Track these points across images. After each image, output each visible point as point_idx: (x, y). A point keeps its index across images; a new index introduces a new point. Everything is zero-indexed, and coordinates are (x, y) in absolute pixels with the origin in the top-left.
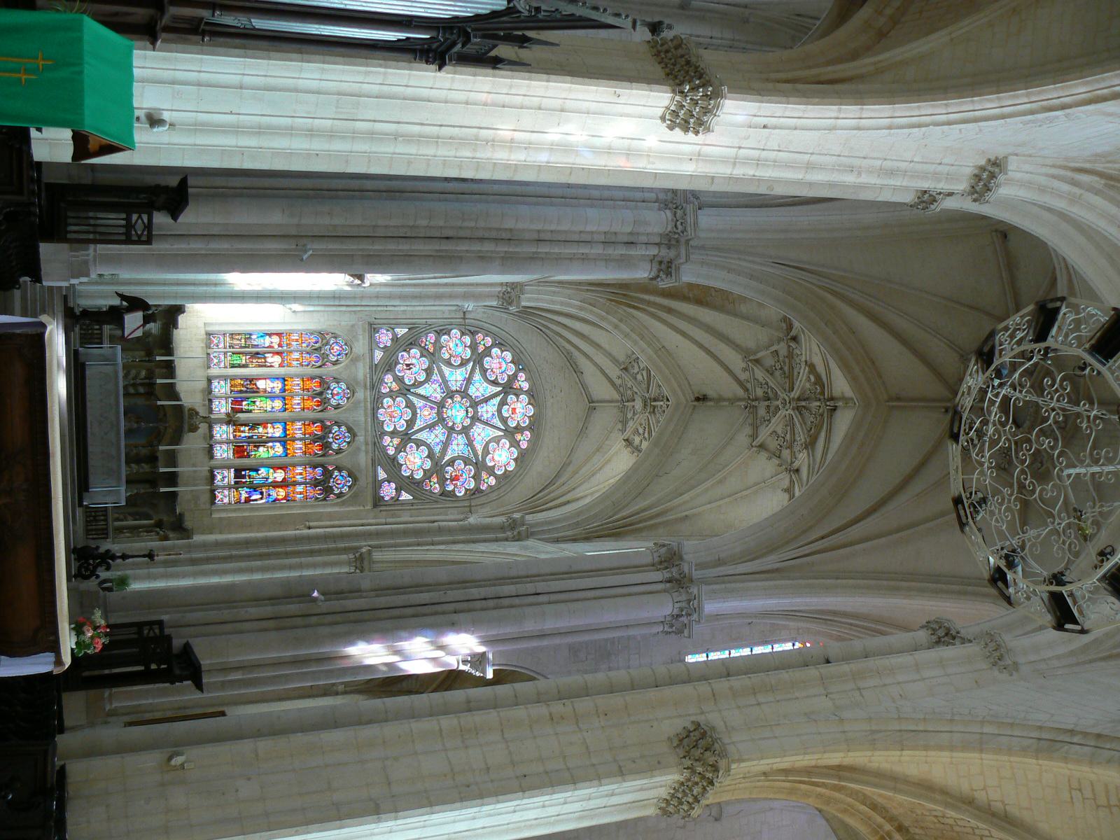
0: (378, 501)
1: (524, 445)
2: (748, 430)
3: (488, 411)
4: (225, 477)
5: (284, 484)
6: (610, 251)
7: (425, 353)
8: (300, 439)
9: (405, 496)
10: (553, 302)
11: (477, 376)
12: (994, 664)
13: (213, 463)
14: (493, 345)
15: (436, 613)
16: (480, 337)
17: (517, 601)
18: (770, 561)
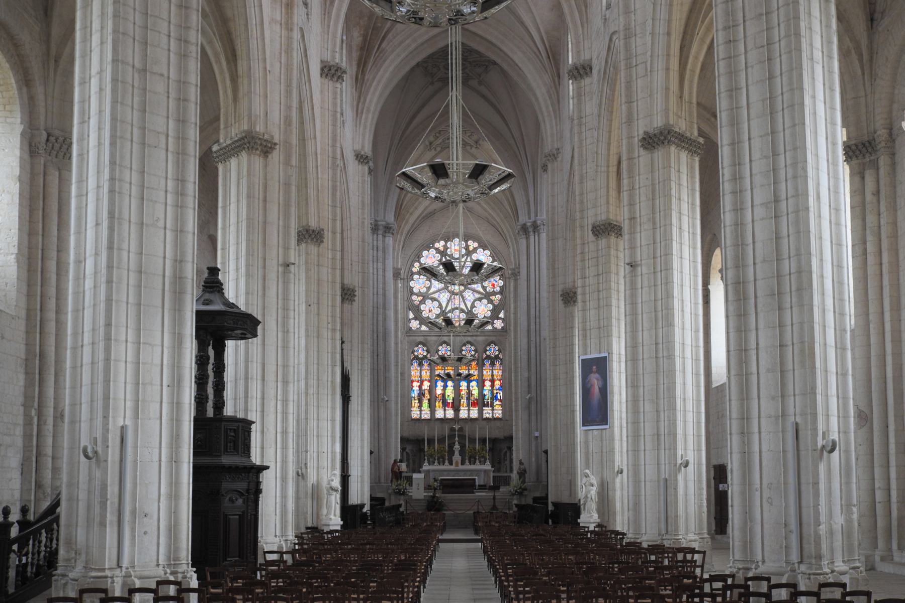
0: (504, 330)
1: (476, 245)
4: (487, 412)
5: (492, 382)
7: (423, 302)
9: (502, 315)
12: (556, 159)
15: (540, 346)
17: (537, 308)
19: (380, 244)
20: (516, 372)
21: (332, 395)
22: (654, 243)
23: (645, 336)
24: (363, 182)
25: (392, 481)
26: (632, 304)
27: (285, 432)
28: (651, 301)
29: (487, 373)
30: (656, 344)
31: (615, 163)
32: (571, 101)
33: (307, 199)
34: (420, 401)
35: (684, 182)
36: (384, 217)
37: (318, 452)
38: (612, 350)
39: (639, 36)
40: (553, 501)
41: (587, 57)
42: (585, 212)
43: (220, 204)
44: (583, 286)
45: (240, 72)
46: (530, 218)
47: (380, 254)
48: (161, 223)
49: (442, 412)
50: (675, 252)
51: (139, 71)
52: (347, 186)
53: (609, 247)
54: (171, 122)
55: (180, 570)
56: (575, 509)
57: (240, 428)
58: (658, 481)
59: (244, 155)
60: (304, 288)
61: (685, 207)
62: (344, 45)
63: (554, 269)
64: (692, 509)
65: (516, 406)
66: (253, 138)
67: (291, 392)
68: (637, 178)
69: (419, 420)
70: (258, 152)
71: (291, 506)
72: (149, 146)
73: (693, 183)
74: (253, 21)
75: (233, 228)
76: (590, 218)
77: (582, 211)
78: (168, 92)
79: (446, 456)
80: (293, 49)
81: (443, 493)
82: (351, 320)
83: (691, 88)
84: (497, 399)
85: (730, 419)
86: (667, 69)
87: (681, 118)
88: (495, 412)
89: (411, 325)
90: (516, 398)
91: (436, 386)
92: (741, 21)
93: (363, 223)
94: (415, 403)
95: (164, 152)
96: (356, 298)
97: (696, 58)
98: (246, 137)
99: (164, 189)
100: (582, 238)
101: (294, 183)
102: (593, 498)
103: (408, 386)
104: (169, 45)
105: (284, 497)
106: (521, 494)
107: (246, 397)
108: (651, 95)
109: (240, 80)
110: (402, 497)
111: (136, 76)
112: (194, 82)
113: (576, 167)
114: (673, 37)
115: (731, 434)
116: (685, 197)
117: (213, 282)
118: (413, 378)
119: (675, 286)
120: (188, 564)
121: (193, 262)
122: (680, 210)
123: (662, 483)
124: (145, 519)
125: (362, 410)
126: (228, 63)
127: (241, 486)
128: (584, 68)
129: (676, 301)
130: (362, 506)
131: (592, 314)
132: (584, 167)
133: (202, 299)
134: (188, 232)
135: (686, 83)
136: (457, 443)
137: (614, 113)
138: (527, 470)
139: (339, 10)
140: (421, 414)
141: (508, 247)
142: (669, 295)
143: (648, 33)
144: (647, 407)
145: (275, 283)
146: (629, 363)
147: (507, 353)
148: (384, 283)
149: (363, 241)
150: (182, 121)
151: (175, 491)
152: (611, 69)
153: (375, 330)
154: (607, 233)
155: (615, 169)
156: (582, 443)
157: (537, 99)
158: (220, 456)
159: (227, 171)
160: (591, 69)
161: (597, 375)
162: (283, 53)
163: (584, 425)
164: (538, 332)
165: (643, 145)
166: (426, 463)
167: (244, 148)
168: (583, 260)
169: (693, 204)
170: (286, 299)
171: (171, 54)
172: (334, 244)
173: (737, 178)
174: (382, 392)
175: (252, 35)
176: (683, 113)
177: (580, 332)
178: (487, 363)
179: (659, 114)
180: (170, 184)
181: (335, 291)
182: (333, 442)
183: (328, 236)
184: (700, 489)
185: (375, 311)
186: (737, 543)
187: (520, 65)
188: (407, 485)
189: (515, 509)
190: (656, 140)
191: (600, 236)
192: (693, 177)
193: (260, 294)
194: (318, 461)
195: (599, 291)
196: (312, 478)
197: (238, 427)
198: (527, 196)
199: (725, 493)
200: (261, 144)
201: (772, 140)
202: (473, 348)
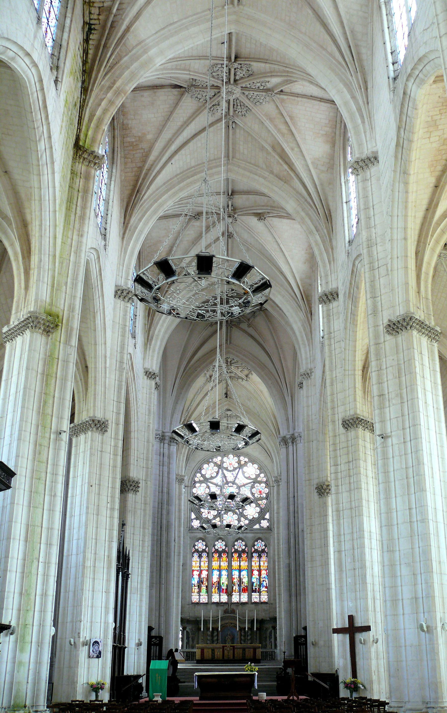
2: (240, 380)
3: (230, 477)
4: (255, 597)
5: (260, 571)
6: (166, 464)
8: (240, 563)
9: (267, 516)
10: (184, 453)
11: (214, 481)
12: (309, 377)
13: (250, 603)
14: (200, 473)
16: (197, 479)
18: (288, 399)
19: (166, 451)
21: (108, 568)
24: (150, 393)
26: (385, 473)
28: (402, 468)
34: (199, 587)
39: (380, 244)
41: (334, 286)
42: (336, 409)
45: (32, 266)
46: (289, 432)
47: (166, 459)
49: (218, 597)
52: (136, 395)
53: (357, 437)
60: (87, 471)
66: (37, 318)
68: (384, 359)
69: (198, 604)
76: (340, 414)
77: (333, 408)
80: (81, 251)
83: (426, 287)
88: (262, 597)
89: (193, 524)
90: (279, 584)
94: (196, 589)
96: (140, 489)
97: (429, 264)
98: (30, 317)
100: (334, 430)
101: (72, 361)
103: (190, 575)
109: (32, 272)
113: (327, 373)
114: (409, 241)
125: (142, 588)
126: (23, 258)
128: (332, 294)
131: (344, 497)
132: (334, 372)
140: (199, 598)
141: (273, 462)
142: (419, 462)
147: (271, 548)
149: (148, 442)
154: (355, 426)
156: (338, 615)
157: (294, 333)
159: (13, 349)
160: (338, 295)
172: (117, 434)
175: (44, 234)
176: (421, 305)
177: (334, 513)
181: (116, 475)
182: (107, 613)
183: (111, 427)
185: (160, 506)
187: (280, 306)
190: (400, 326)
191: (349, 429)
195: (350, 476)
198: (286, 414)
202: (244, 543)
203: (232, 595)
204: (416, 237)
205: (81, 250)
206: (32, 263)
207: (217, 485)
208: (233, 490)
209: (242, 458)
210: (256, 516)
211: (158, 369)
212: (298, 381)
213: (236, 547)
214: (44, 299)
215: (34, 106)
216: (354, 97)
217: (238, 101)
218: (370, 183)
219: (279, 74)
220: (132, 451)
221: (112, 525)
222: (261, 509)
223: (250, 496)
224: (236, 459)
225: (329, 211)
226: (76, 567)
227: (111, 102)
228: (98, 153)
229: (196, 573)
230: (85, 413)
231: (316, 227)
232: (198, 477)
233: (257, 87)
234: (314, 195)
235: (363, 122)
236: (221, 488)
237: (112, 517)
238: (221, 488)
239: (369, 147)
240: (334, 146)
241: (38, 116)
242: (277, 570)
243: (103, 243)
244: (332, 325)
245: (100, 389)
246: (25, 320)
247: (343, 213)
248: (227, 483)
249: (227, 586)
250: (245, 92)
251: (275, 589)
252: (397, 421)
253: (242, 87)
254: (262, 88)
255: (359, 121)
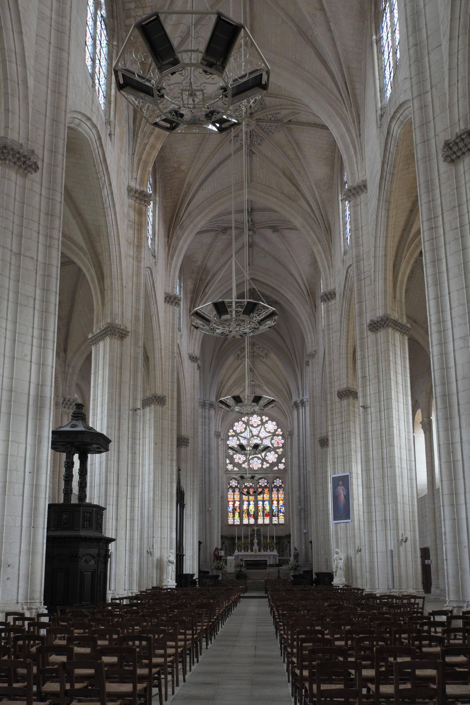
1: (267, 418)
3: (255, 431)
4: (275, 521)
5: (278, 501)
6: (207, 424)
9: (283, 461)
14: (233, 429)
16: (230, 434)
17: (305, 453)
19: (207, 414)
20: (292, 494)
22: (379, 392)
23: (374, 454)
24: (194, 373)
25: (214, 561)
27: (132, 520)
28: (378, 430)
29: (274, 496)
30: (382, 459)
31: (352, 352)
32: (323, 320)
33: (155, 378)
34: (234, 514)
35: (398, 352)
36: (209, 398)
37: (161, 538)
38: (352, 471)
40: (316, 572)
41: (332, 287)
43: (93, 372)
44: (333, 431)
45: (106, 288)
46: (299, 398)
47: (207, 420)
48: (28, 358)
49: (247, 520)
50: (393, 397)
51: (16, 254)
53: (349, 405)
54: (38, 290)
55: (34, 607)
56: (330, 576)
57: (94, 511)
58: (386, 552)
59: (108, 339)
61: (399, 368)
62: (182, 289)
63: (314, 425)
64: (410, 572)
65: (293, 515)
66: (113, 327)
67: (137, 493)
69: (233, 525)
70: (116, 337)
71: (136, 569)
72: (21, 304)
73: (404, 353)
74: (114, 254)
75: (100, 386)
76: (336, 388)
77: (331, 383)
78: (36, 270)
79: (249, 546)
81: (247, 569)
82: (186, 458)
83: (401, 293)
84: (281, 512)
85: (442, 495)
86: (385, 279)
87: (395, 311)
88: (280, 520)
89: (228, 467)
91: (243, 504)
92: (440, 213)
93: (194, 398)
94: (231, 515)
95: (32, 310)
96: (189, 444)
97: (404, 273)
98: (109, 327)
99: (31, 335)
100: (331, 400)
102: (342, 567)
104: (38, 239)
105: (131, 563)
106: (295, 569)
107: (106, 495)
108: (374, 296)
109: (106, 292)
110: (220, 571)
111: (13, 257)
112: (56, 264)
113: (327, 356)
115: (443, 506)
116: (399, 361)
117: (79, 413)
118: (229, 500)
119: (394, 419)
120: (41, 602)
121: (51, 386)
122: (396, 370)
123: (389, 553)
124: (8, 568)
125: (193, 514)
126: (99, 281)
127: (94, 551)
129: (395, 429)
130: (193, 575)
131: (338, 448)
132: (332, 355)
133: (70, 424)
134: (48, 365)
135: (398, 290)
136: (256, 538)
137: (350, 320)
138: (300, 554)
139: (177, 263)
140: (234, 521)
142: (390, 426)
143: (371, 258)
144: (377, 502)
145: (127, 421)
146: (364, 472)
147: (287, 484)
148: (209, 438)
150: (46, 290)
151: (32, 548)
152: (348, 291)
153: (204, 467)
154: (347, 396)
155: (351, 356)
157: (302, 322)
158: (79, 530)
159: (97, 350)
160: (335, 294)
161: (342, 487)
162: (134, 277)
163: (334, 520)
164: (305, 468)
165: (370, 329)
166: (236, 551)
167: (108, 334)
168: (332, 414)
169: (405, 367)
170: (134, 432)
171: (40, 244)
172: (172, 406)
173: (441, 321)
174: (207, 505)
177: (331, 460)
178: (275, 490)
179: (380, 308)
180: (36, 332)
181: (173, 435)
182: (171, 532)
183: (169, 401)
184: (416, 558)
185: (204, 455)
186: (451, 588)
187: (291, 300)
188: (224, 564)
189: (292, 578)
190: (378, 324)
192: (404, 350)
193: (117, 428)
194: (161, 544)
196: (157, 554)
197: (93, 511)
199: (429, 566)
200: (119, 332)
201: (466, 292)
203: (258, 519)
204: (394, 253)
205: (141, 273)
206: (106, 285)
207: (245, 438)
208: (257, 441)
209: (264, 417)
210: (275, 460)
211: (199, 354)
212: (305, 360)
213: (260, 484)
214: (117, 313)
215: (97, 160)
216: (348, 130)
217: (254, 132)
218: (359, 208)
219: (287, 107)
220: (183, 416)
221: (172, 471)
222: (279, 455)
223: (270, 445)
224: (259, 418)
225: (329, 224)
226: (149, 500)
227: (153, 147)
228: (147, 192)
229: (231, 504)
230: (148, 391)
231: (318, 239)
232: (231, 432)
233: (269, 118)
234: (317, 212)
235: (356, 153)
236: (249, 440)
237: (172, 466)
238: (249, 440)
239: (360, 176)
240: (333, 168)
241: (101, 168)
242: (290, 500)
243: (154, 260)
244: (330, 319)
245: (158, 373)
246: (104, 329)
247: (340, 227)
248: (253, 436)
249: (254, 512)
250: (259, 124)
251: (289, 514)
252: (375, 396)
253: (257, 119)
254: (273, 119)
255: (353, 152)
